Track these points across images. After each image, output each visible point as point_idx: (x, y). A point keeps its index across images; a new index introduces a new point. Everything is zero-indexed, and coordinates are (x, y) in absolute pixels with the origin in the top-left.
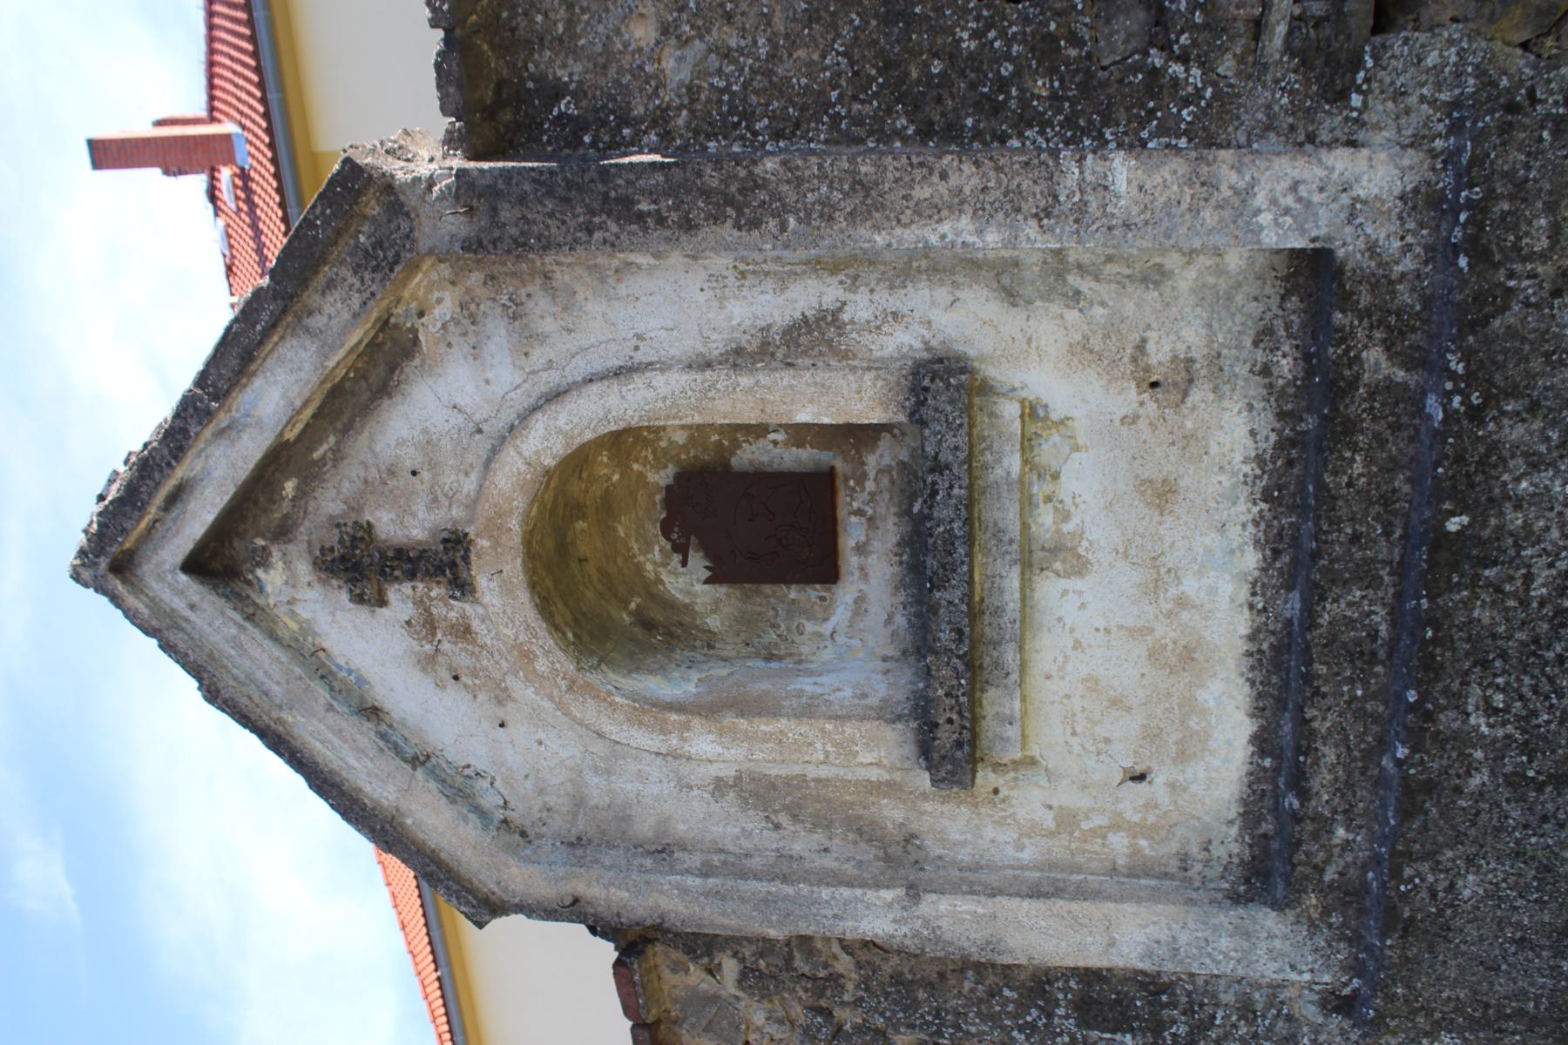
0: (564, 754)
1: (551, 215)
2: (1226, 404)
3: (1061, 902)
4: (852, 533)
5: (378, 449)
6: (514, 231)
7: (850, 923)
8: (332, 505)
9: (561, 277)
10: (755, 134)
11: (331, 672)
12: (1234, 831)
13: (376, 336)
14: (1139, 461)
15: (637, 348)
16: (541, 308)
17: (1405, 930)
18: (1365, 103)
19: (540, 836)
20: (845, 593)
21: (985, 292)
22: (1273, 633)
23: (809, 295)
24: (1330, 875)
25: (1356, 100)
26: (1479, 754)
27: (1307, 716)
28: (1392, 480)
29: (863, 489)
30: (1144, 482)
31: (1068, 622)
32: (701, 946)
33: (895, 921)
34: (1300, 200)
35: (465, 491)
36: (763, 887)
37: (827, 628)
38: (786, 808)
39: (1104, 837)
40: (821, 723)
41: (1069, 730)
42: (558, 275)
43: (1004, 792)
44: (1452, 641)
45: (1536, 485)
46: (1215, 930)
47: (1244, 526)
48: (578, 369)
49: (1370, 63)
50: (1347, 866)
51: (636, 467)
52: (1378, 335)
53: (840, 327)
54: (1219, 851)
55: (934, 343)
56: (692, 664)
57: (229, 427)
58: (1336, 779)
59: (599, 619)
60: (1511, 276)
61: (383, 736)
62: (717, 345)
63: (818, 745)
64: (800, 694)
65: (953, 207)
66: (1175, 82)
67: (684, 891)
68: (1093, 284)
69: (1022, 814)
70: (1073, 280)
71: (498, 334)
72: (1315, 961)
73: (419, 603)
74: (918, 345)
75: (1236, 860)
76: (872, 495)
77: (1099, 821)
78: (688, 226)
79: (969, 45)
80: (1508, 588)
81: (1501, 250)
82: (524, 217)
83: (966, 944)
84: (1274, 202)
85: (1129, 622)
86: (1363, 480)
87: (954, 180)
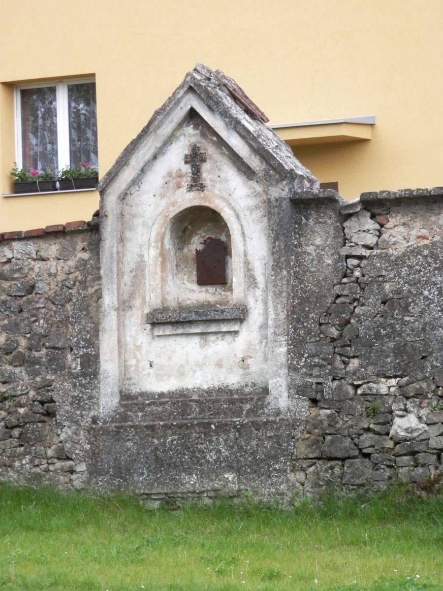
0: (147, 212)
1: (276, 221)
4: (211, 289)
6: (272, 211)
10: (295, 268)
12: (138, 390)
17: (117, 431)
19: (123, 203)
20: (195, 287)
23: (261, 279)
24: (129, 413)
25: (297, 396)
26: (162, 440)
31: (189, 345)
32: (95, 247)
33: (109, 305)
36: (115, 269)
38: (136, 274)
40: (160, 284)
48: (244, 222)
52: (252, 407)
53: (254, 288)
54: (132, 388)
56: (174, 245)
61: (149, 161)
62: (249, 258)
64: (167, 277)
65: (277, 314)
66: (301, 360)
70: (265, 341)
71: (252, 202)
74: (251, 306)
76: (221, 294)
78: (273, 254)
79: (311, 316)
84: (278, 382)
87: (281, 313)
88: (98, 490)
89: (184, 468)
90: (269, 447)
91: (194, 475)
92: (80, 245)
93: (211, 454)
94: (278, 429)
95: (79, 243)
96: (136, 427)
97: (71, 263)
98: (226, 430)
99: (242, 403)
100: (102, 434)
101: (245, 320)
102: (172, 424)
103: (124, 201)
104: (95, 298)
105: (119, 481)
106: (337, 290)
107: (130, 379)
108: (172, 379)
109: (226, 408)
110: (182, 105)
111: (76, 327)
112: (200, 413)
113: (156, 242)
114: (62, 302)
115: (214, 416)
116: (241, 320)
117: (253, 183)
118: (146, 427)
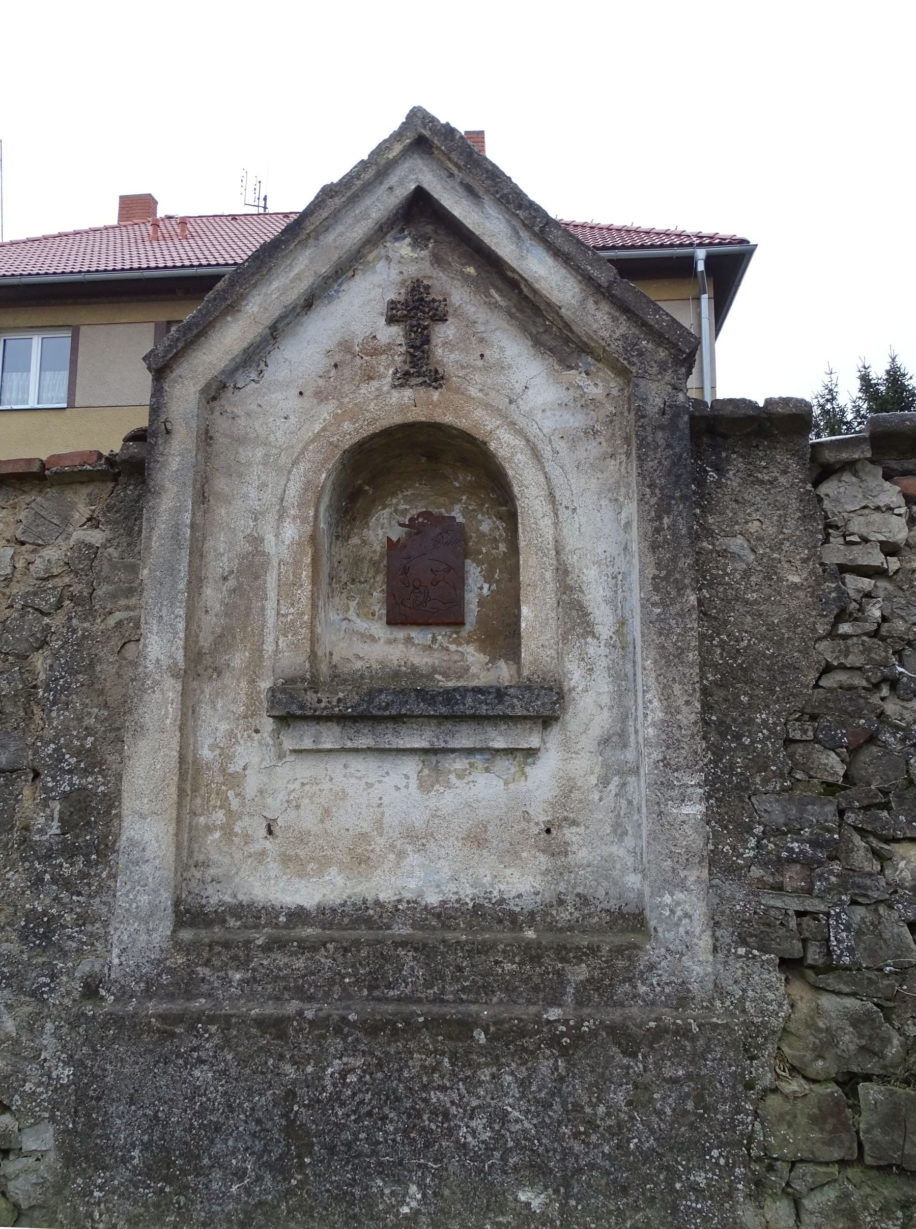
1: (660, 463)
2: (539, 878)
3: (176, 779)
4: (420, 636)
5: (498, 333)
6: (650, 439)
7: (155, 628)
8: (458, 297)
9: (612, 464)
11: (338, 278)
12: (228, 899)
13: (574, 343)
14: (499, 823)
15: (567, 508)
16: (592, 449)
17: (165, 1032)
18: (741, 956)
20: (379, 629)
21: (608, 726)
22: (381, 917)
23: (603, 618)
24: (202, 971)
25: (742, 951)
26: (310, 1069)
27: (328, 945)
28: (500, 990)
29: (450, 643)
30: (486, 827)
31: (386, 779)
32: (129, 519)
33: (158, 660)
34: (680, 919)
35: (470, 388)
36: (184, 567)
37: (352, 614)
38: (240, 585)
39: (221, 807)
41: (305, 781)
42: (613, 462)
43: (256, 737)
44: (395, 1041)
45: (509, 1086)
46: (155, 891)
47: (456, 893)
49: (764, 958)
50: (210, 983)
51: (464, 498)
52: (596, 973)
53: (583, 636)
55: (574, 694)
57: (519, 238)
58: (280, 970)
59: (375, 466)
60: (644, 1057)
62: (572, 559)
63: (291, 610)
65: (658, 709)
67: (178, 511)
68: (613, 792)
69: (240, 749)
70: (616, 780)
71: (576, 421)
72: (128, 966)
73: (389, 347)
74: (572, 683)
75: (204, 902)
76: (447, 649)
77: (235, 804)
80: (436, 1075)
81: (662, 1048)
82: (659, 446)
83: (140, 711)
84: (678, 904)
85: (386, 820)
86: (500, 971)
87: (684, 709)
88: (90, 1215)
89: (380, 1164)
90: (668, 1111)
91: (413, 1189)
92: (82, 511)
93: (473, 1124)
94: (698, 1057)
95: (81, 507)
96: (226, 1022)
97: (53, 554)
98: (524, 1049)
99: (563, 960)
100: (115, 1038)
101: (557, 719)
102: (344, 1019)
103: (216, 404)
104: (116, 642)
105: (162, 1190)
106: (826, 651)
107: (206, 865)
108: (334, 871)
109: (513, 974)
110: (392, 180)
111: (54, 714)
112: (428, 985)
113: (301, 505)
114: (22, 647)
115: (472, 997)
116: (547, 721)
117: (577, 377)
118: (262, 1023)
